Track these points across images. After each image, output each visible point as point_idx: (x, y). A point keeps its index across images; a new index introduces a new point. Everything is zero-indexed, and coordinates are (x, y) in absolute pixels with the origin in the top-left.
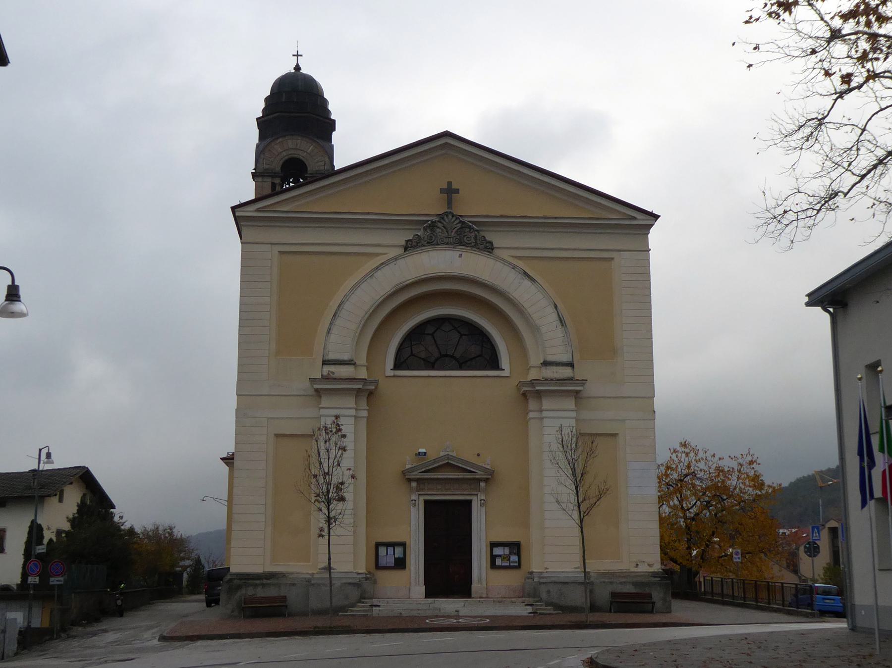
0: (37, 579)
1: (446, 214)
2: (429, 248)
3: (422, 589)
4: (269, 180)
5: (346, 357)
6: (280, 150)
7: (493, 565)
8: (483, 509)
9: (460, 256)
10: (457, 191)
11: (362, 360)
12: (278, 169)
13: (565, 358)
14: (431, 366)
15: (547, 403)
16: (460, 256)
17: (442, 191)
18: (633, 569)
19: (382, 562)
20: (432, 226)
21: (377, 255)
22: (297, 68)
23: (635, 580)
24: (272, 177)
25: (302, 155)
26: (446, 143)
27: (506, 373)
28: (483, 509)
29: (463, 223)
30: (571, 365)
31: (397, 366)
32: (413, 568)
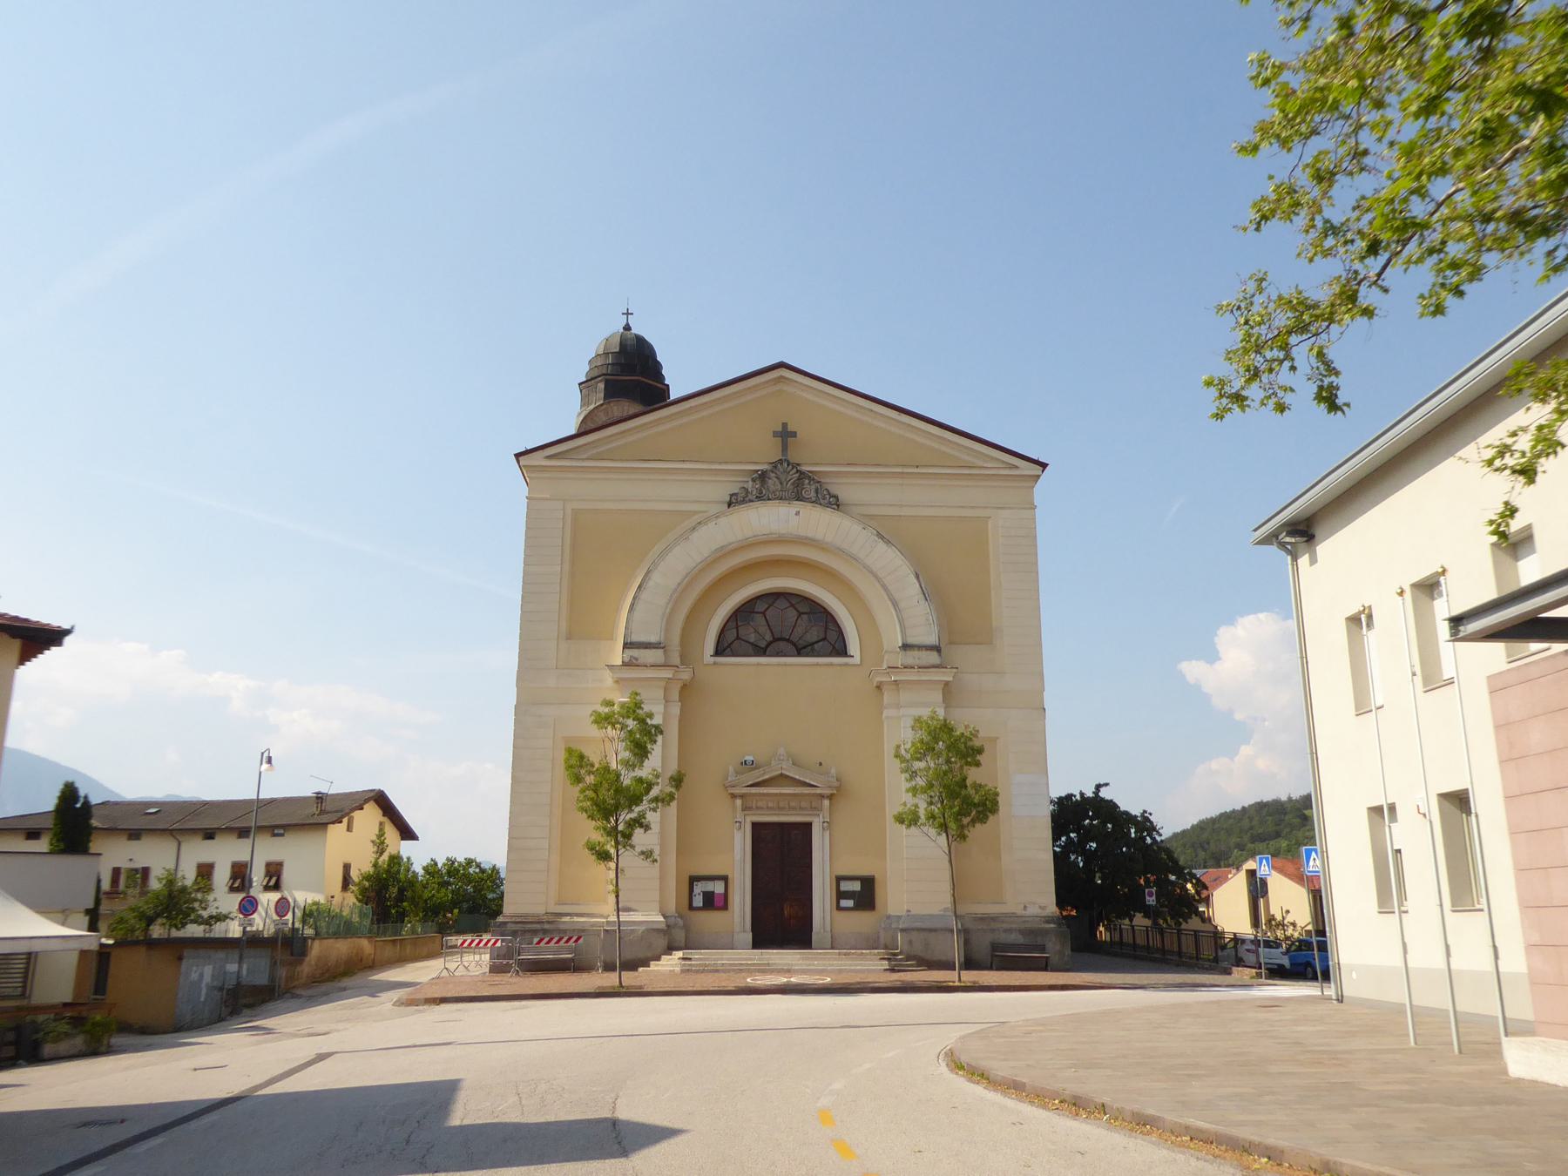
3: (750, 936)
5: (653, 639)
7: (839, 908)
9: (798, 513)
10: (794, 434)
13: (932, 639)
16: (798, 513)
20: (762, 476)
21: (695, 513)
22: (627, 328)
23: (1023, 926)
29: (801, 473)
30: (937, 649)
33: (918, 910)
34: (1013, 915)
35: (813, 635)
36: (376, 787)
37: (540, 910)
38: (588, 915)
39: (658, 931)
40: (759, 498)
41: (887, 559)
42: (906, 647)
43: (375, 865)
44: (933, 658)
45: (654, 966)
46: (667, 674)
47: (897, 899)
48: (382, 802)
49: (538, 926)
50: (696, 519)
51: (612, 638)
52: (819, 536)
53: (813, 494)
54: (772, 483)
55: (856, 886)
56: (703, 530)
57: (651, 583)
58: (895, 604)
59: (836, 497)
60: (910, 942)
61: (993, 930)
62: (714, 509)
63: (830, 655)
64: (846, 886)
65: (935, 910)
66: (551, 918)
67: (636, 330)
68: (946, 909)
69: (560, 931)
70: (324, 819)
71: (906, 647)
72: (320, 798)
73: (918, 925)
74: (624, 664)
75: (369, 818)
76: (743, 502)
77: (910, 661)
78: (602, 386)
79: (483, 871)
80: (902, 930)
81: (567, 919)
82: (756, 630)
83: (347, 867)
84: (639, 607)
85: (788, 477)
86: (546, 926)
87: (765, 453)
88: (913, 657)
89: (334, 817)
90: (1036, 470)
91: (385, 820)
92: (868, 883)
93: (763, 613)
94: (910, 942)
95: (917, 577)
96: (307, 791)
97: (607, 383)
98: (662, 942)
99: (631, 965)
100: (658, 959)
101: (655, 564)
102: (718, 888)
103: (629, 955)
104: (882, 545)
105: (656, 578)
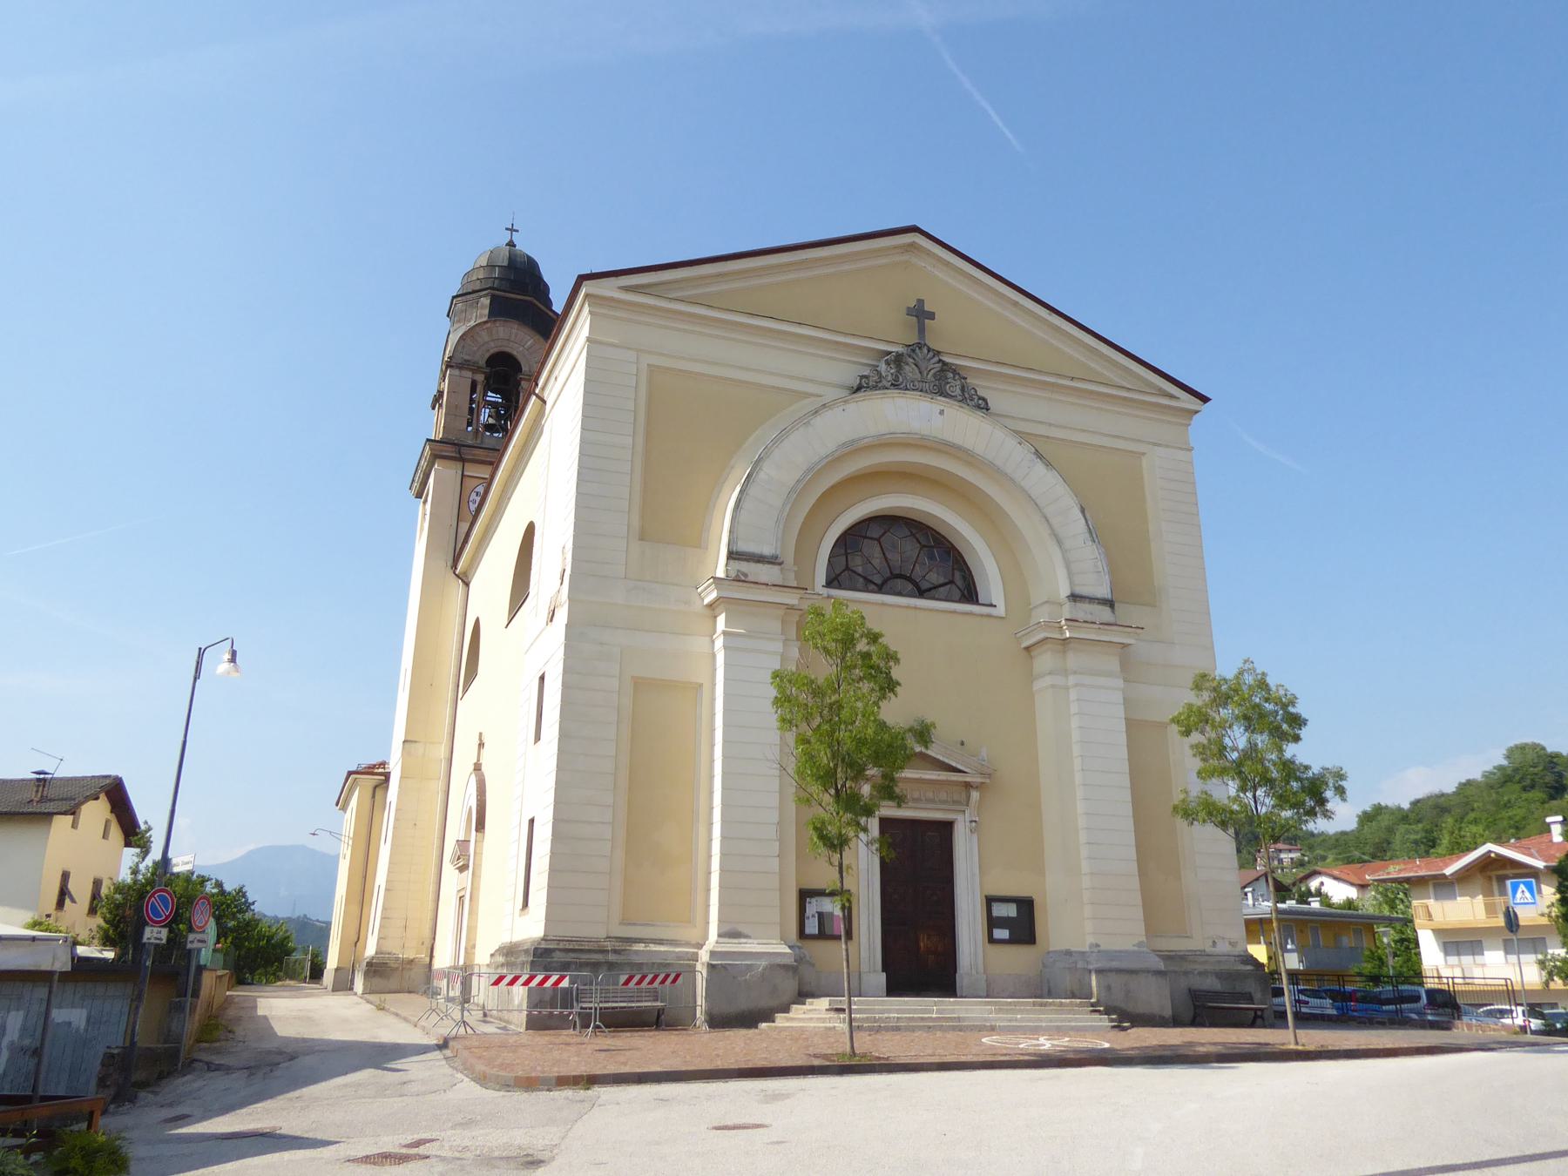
0: (164, 933)
1: (920, 346)
2: (894, 392)
3: (882, 978)
4: (469, 374)
5: (767, 551)
6: (487, 339)
7: (992, 940)
8: (975, 837)
9: (942, 412)
10: (931, 316)
11: (789, 558)
12: (482, 363)
13: (1103, 591)
14: (880, 589)
15: (1073, 659)
16: (942, 412)
17: (910, 311)
18: (1209, 949)
19: (808, 931)
20: (898, 360)
21: (807, 395)
22: (511, 244)
23: (1217, 968)
24: (474, 372)
25: (516, 351)
26: (913, 245)
27: (1001, 610)
28: (975, 837)
29: (944, 364)
30: (1110, 603)
31: (830, 584)
32: (864, 940)
33: (1108, 944)
34: (1203, 953)
35: (934, 578)
36: (113, 773)
37: (599, 932)
38: (660, 942)
39: (785, 967)
40: (895, 385)
41: (1042, 481)
42: (1075, 597)
43: (135, 872)
44: (1104, 613)
45: (781, 1020)
46: (791, 599)
47: (1070, 926)
48: (116, 795)
49: (599, 957)
50: (819, 402)
51: (698, 541)
52: (968, 444)
53: (958, 391)
54: (910, 371)
55: (1010, 911)
56: (827, 415)
57: (762, 475)
58: (1059, 542)
59: (984, 400)
60: (1109, 988)
61: (1186, 973)
62: (830, 394)
63: (959, 601)
64: (1001, 910)
65: (1128, 944)
66: (618, 946)
67: (525, 246)
68: (1140, 944)
69: (632, 965)
70: (49, 807)
71: (1075, 597)
72: (42, 782)
73: (1115, 964)
74: (728, 578)
75: (97, 812)
76: (875, 388)
77: (1081, 616)
78: (486, 301)
79: (223, 892)
80: (1099, 972)
81: (640, 947)
82: (873, 556)
83: (65, 876)
84: (746, 505)
85: (919, 362)
86: (611, 957)
87: (897, 336)
88: (1084, 611)
89: (65, 806)
90: (1192, 403)
91: (113, 818)
92: (1026, 906)
93: (878, 540)
94: (1109, 988)
95: (1083, 511)
96: (27, 774)
97: (494, 299)
98: (790, 985)
99: (749, 1019)
100: (786, 1010)
101: (767, 453)
102: (832, 907)
103: (743, 1003)
104: (1040, 467)
105: (768, 471)
